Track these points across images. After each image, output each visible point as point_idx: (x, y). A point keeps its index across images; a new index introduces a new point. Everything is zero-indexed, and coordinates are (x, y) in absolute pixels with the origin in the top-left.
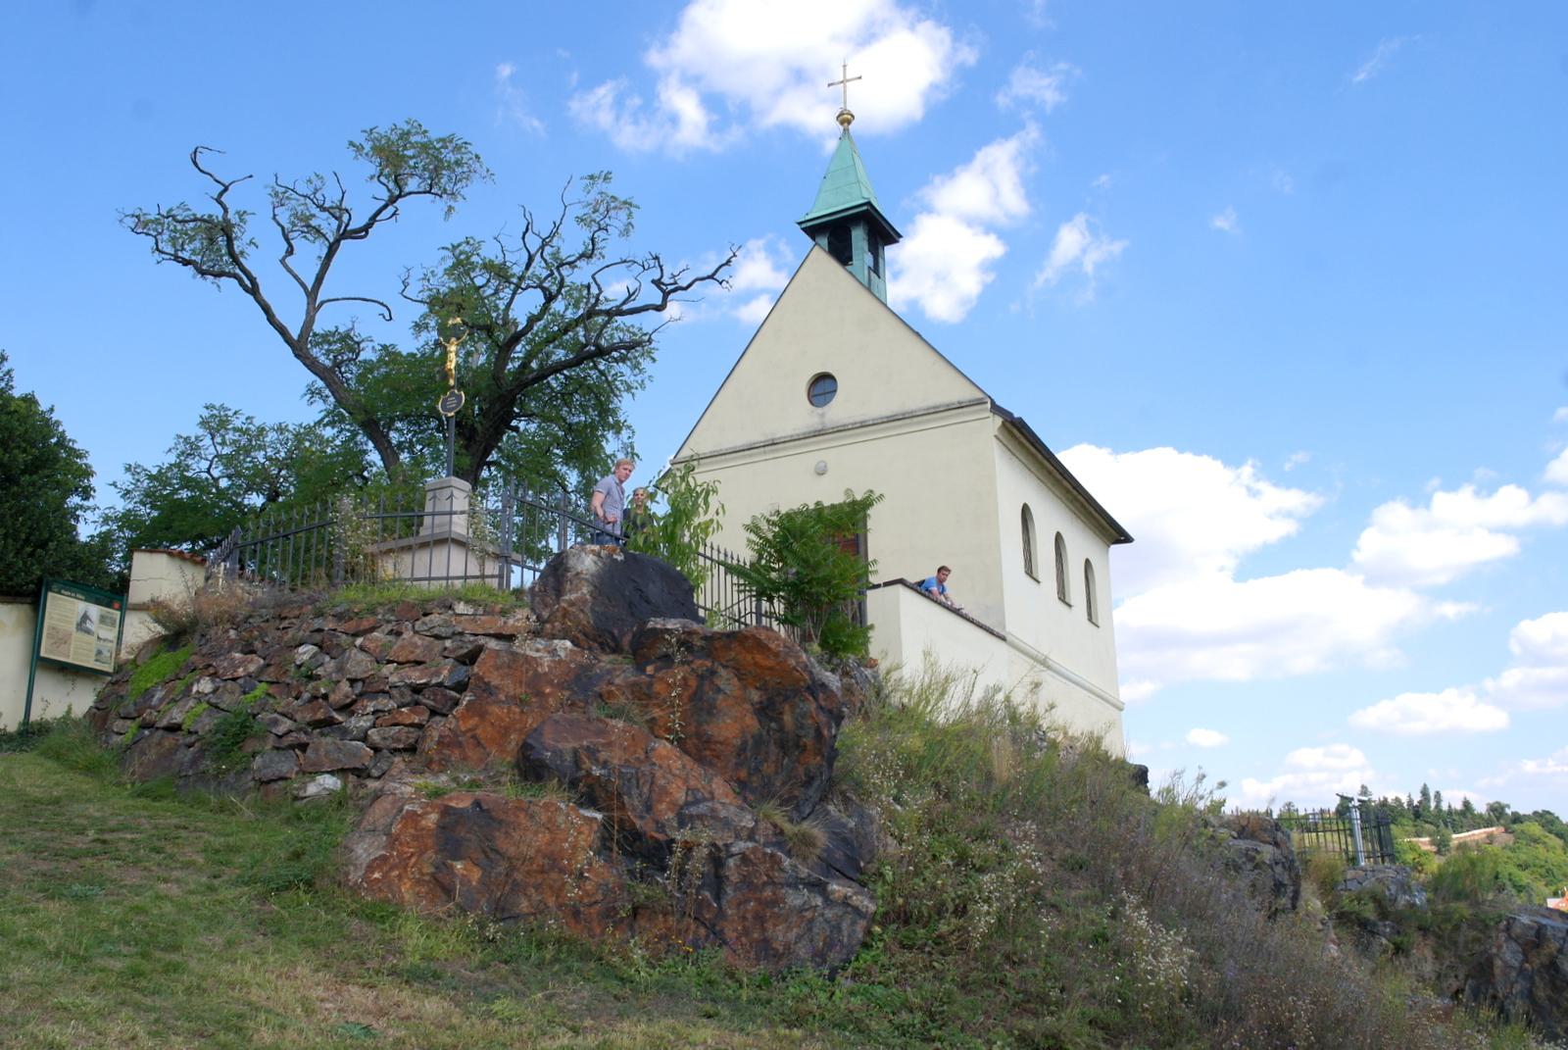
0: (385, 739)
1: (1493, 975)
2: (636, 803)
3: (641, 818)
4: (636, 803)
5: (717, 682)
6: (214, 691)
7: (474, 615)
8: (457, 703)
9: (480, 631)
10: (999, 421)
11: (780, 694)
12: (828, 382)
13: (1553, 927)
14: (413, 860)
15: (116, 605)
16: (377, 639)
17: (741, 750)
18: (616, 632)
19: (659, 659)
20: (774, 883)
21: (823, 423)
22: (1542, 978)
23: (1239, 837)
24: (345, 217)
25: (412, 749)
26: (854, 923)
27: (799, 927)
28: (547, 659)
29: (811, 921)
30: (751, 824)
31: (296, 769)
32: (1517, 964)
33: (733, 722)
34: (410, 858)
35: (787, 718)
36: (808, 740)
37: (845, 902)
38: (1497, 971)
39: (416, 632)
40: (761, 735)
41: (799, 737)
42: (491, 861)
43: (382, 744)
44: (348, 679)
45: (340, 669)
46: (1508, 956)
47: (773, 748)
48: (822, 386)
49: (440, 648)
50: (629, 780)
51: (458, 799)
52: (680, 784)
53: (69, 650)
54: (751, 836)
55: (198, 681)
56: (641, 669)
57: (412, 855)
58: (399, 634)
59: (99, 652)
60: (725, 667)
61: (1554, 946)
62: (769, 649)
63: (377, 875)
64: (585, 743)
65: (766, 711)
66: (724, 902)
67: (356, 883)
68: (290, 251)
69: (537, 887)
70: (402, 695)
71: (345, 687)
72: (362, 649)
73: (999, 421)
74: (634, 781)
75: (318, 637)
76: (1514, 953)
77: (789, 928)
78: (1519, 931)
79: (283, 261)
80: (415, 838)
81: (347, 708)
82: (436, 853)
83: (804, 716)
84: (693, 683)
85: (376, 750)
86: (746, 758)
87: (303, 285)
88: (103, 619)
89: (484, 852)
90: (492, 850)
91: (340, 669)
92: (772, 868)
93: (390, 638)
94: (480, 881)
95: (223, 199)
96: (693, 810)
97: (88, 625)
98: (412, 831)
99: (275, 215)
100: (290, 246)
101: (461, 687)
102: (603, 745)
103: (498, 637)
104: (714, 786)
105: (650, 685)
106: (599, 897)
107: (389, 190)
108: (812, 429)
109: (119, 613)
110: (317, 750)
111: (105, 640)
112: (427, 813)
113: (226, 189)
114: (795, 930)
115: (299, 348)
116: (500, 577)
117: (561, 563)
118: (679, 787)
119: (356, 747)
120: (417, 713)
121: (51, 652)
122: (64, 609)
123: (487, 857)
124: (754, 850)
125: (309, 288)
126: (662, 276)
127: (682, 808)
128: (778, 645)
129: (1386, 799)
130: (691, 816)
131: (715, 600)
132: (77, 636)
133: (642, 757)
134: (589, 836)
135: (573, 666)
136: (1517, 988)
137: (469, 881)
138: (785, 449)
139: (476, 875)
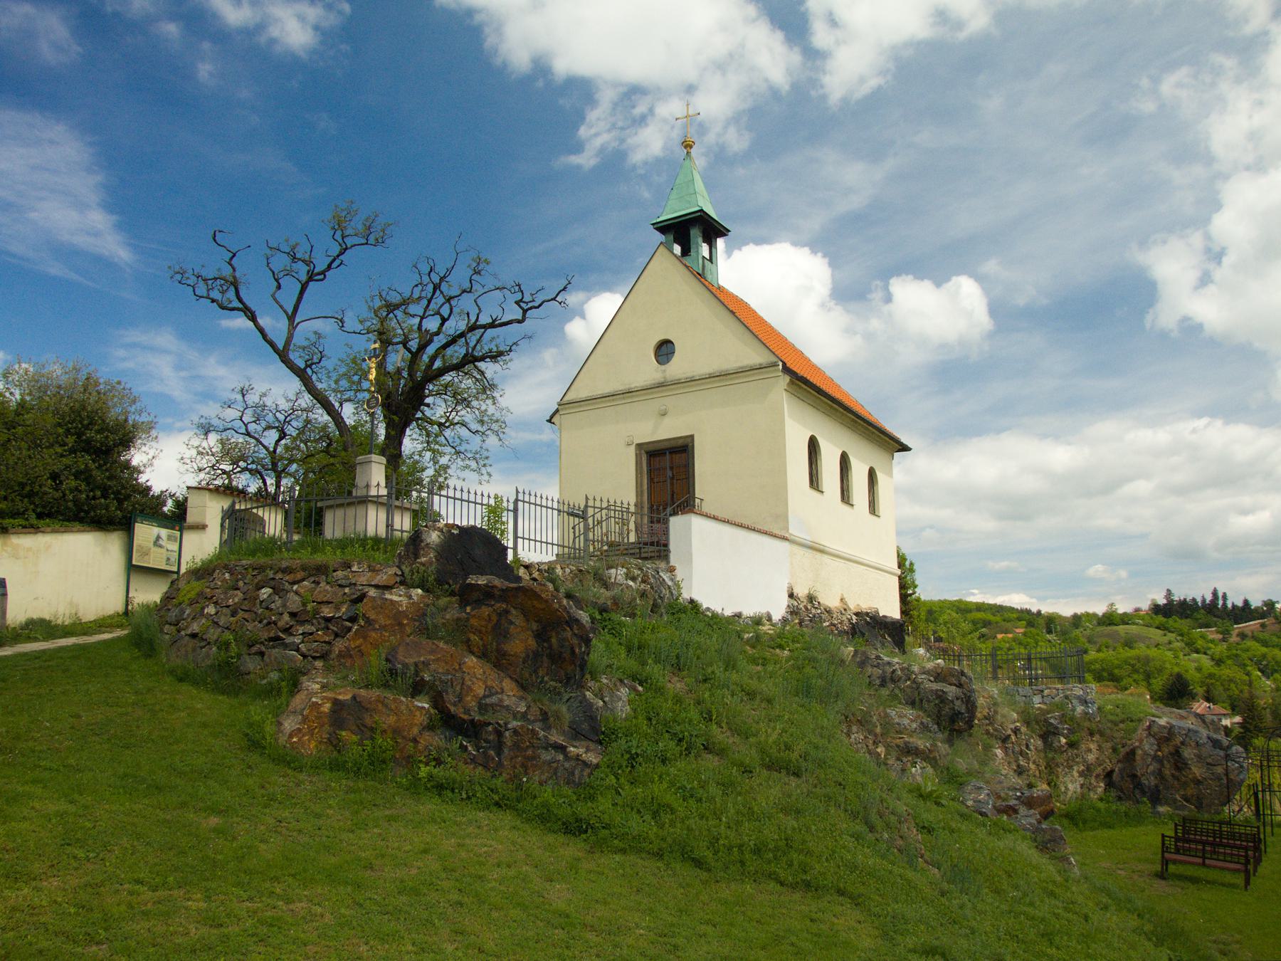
0: (309, 650)
1: (1135, 761)
3: (455, 705)
6: (217, 613)
8: (350, 629)
12: (669, 345)
14: (316, 730)
15: (177, 528)
16: (306, 586)
21: (665, 378)
22: (1169, 761)
25: (324, 657)
26: (582, 770)
29: (556, 769)
30: (524, 709)
32: (1152, 753)
33: (521, 642)
34: (314, 729)
35: (554, 640)
36: (567, 655)
37: (578, 757)
38: (1138, 758)
39: (328, 583)
43: (308, 653)
45: (284, 605)
46: (1147, 747)
48: (664, 350)
49: (342, 593)
51: (344, 693)
52: (481, 684)
53: (149, 559)
54: (524, 716)
55: (208, 606)
57: (316, 727)
58: (318, 583)
59: (168, 559)
61: (1179, 739)
64: (422, 659)
65: (541, 636)
66: (502, 757)
68: (279, 287)
70: (319, 623)
71: (286, 617)
72: (296, 593)
73: (787, 378)
74: (449, 683)
75: (272, 583)
76: (1152, 745)
77: (542, 773)
79: (273, 296)
80: (317, 718)
82: (330, 726)
85: (304, 656)
87: (285, 312)
88: (170, 538)
89: (358, 726)
90: (363, 725)
91: (284, 605)
93: (313, 585)
95: (232, 262)
96: (488, 701)
97: (161, 542)
99: (268, 264)
100: (279, 284)
101: (353, 619)
103: (377, 587)
104: (504, 684)
105: (468, 620)
107: (340, 245)
108: (657, 381)
110: (270, 656)
111: (172, 551)
112: (324, 703)
113: (234, 255)
114: (546, 774)
115: (283, 356)
117: (418, 537)
118: (480, 686)
119: (292, 655)
121: (139, 561)
122: (145, 532)
123: (360, 729)
124: (522, 727)
125: (290, 314)
127: (481, 699)
128: (548, 595)
129: (1185, 600)
132: (154, 549)
133: (457, 668)
135: (422, 605)
136: (1151, 768)
138: (637, 396)
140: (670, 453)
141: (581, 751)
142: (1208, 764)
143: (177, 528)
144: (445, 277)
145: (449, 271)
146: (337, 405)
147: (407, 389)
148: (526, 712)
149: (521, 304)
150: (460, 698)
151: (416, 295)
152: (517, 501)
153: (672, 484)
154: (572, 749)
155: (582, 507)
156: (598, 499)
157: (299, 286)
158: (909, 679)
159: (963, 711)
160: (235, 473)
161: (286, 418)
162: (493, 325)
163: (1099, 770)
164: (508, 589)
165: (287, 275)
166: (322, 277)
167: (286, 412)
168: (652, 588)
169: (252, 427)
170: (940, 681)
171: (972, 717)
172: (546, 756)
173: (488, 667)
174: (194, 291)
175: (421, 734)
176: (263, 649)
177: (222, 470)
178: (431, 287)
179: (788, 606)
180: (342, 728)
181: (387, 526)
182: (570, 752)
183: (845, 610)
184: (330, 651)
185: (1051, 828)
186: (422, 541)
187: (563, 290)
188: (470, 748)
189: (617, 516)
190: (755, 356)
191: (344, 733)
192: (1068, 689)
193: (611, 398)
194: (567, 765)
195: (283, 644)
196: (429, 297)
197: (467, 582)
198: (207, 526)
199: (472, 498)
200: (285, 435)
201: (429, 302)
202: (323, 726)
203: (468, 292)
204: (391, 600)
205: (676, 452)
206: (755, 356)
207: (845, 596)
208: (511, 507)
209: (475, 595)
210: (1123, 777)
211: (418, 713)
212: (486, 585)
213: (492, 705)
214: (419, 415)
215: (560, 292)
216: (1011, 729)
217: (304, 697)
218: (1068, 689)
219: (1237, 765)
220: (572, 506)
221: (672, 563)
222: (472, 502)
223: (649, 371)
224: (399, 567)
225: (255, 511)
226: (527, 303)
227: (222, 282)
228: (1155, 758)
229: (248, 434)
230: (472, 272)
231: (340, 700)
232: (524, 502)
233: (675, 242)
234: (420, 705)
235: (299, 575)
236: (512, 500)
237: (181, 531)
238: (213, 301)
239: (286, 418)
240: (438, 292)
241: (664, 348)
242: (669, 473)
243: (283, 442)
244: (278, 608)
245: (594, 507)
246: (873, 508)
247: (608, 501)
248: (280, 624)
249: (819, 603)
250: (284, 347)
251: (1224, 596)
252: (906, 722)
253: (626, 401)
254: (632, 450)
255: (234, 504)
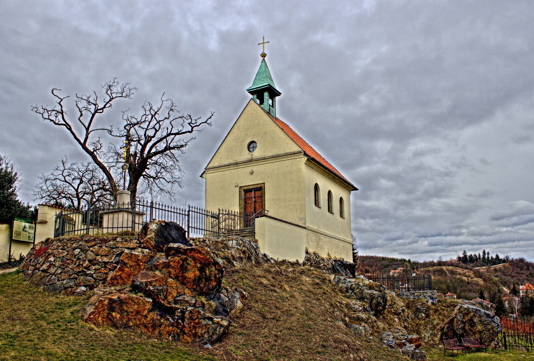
0: (97, 277)
2: (162, 297)
3: (164, 300)
4: (162, 297)
5: (188, 262)
6: (54, 261)
7: (122, 242)
9: (123, 247)
10: (306, 158)
11: (205, 265)
12: (254, 144)
13: (472, 309)
14: (102, 312)
17: (195, 280)
18: (161, 246)
19: (172, 255)
20: (199, 318)
21: (252, 158)
22: (468, 323)
23: (369, 289)
24: (97, 106)
26: (220, 328)
27: (205, 329)
28: (141, 255)
31: (74, 284)
32: (461, 320)
34: (101, 312)
35: (207, 272)
37: (218, 323)
38: (455, 322)
40: (200, 276)
41: (211, 277)
42: (123, 312)
44: (88, 260)
45: (86, 257)
47: (203, 280)
48: (251, 146)
50: (160, 291)
53: (20, 237)
56: (167, 258)
57: (101, 311)
58: (102, 247)
59: (29, 237)
60: (190, 257)
62: (202, 253)
63: (92, 316)
64: (149, 280)
65: (202, 270)
67: (86, 319)
68: (81, 115)
69: (135, 319)
71: (87, 262)
72: (92, 251)
77: (202, 330)
78: (463, 310)
79: (79, 119)
81: (88, 268)
83: (211, 271)
84: (181, 262)
86: (196, 282)
87: (85, 126)
92: (198, 314)
93: (99, 248)
94: (119, 318)
96: (178, 298)
98: (101, 305)
99: (77, 104)
102: (154, 281)
103: (128, 248)
104: (185, 291)
106: (151, 322)
107: (110, 97)
109: (34, 225)
110: (79, 280)
112: (105, 300)
113: (62, 100)
114: (204, 330)
116: (132, 227)
117: (147, 226)
120: (106, 270)
122: (18, 224)
123: (121, 311)
124: (193, 310)
126: (192, 121)
127: (175, 297)
130: (178, 300)
131: (208, 218)
132: (22, 232)
133: (165, 284)
134: (148, 306)
136: (461, 326)
137: (117, 318)
139: (118, 316)
140: (254, 191)
141: (219, 320)
142: (484, 324)
143: (34, 223)
144: (157, 112)
145: (159, 109)
146: (108, 168)
147: (139, 161)
148: (195, 303)
149: (191, 124)
150: (166, 297)
151: (143, 120)
152: (189, 211)
153: (255, 204)
154: (215, 319)
155: (217, 214)
156: (224, 210)
157: (91, 115)
158: (358, 289)
159: (382, 302)
160: (59, 199)
161: (83, 174)
162: (178, 134)
163: (438, 327)
164: (187, 249)
165: (85, 110)
166: (101, 111)
167: (83, 171)
168: (248, 249)
169: (67, 178)
170: (372, 289)
171: (386, 304)
172: (204, 322)
173: (178, 284)
174: (43, 116)
175: (149, 313)
176: (76, 276)
177: (53, 197)
178: (150, 117)
179: (306, 257)
180: (113, 311)
181: (132, 222)
182: (215, 320)
183: (330, 259)
184: (107, 277)
185: (420, 352)
186: (148, 228)
187: (210, 118)
188: (170, 319)
189: (232, 218)
190: (295, 148)
191: (114, 314)
192: (425, 293)
193: (228, 166)
194: (213, 326)
195: (86, 274)
196: (149, 120)
197: (169, 246)
198: (47, 222)
199: (178, 212)
200: (83, 182)
201: (150, 122)
202: (104, 310)
203: (167, 119)
204: (135, 254)
205: (257, 191)
206: (295, 148)
207: (330, 253)
208: (187, 213)
209: (173, 252)
210: (448, 330)
211: (147, 304)
212: (178, 248)
213: (180, 300)
214: (144, 173)
215: (208, 119)
216: (401, 310)
217: (96, 298)
218: (425, 293)
219: (496, 325)
220: (213, 213)
221: (256, 238)
222: (170, 211)
223: (246, 155)
224: (138, 240)
225: (69, 215)
226: (193, 124)
227: (56, 112)
228: (462, 322)
229: (66, 181)
230: (169, 110)
231: (112, 299)
232: (192, 211)
233: (270, 99)
234: (148, 300)
235: (93, 243)
236: (187, 210)
237: (35, 224)
238: (51, 120)
239: (83, 174)
240: (154, 118)
241: (252, 146)
242: (254, 200)
243: (81, 185)
244: (83, 258)
245: (223, 214)
246: (342, 215)
247: (229, 211)
248: (84, 265)
249: (319, 256)
250: (84, 142)
251: (488, 253)
252: (357, 306)
253: (235, 168)
254: (237, 189)
255: (62, 212)
